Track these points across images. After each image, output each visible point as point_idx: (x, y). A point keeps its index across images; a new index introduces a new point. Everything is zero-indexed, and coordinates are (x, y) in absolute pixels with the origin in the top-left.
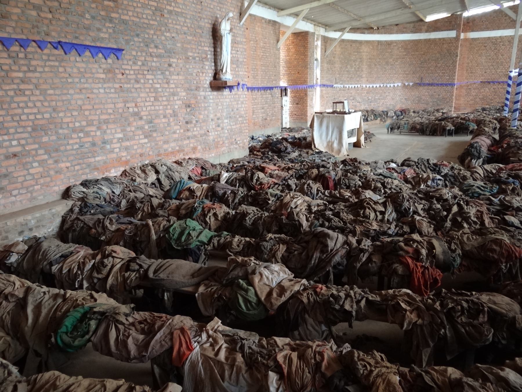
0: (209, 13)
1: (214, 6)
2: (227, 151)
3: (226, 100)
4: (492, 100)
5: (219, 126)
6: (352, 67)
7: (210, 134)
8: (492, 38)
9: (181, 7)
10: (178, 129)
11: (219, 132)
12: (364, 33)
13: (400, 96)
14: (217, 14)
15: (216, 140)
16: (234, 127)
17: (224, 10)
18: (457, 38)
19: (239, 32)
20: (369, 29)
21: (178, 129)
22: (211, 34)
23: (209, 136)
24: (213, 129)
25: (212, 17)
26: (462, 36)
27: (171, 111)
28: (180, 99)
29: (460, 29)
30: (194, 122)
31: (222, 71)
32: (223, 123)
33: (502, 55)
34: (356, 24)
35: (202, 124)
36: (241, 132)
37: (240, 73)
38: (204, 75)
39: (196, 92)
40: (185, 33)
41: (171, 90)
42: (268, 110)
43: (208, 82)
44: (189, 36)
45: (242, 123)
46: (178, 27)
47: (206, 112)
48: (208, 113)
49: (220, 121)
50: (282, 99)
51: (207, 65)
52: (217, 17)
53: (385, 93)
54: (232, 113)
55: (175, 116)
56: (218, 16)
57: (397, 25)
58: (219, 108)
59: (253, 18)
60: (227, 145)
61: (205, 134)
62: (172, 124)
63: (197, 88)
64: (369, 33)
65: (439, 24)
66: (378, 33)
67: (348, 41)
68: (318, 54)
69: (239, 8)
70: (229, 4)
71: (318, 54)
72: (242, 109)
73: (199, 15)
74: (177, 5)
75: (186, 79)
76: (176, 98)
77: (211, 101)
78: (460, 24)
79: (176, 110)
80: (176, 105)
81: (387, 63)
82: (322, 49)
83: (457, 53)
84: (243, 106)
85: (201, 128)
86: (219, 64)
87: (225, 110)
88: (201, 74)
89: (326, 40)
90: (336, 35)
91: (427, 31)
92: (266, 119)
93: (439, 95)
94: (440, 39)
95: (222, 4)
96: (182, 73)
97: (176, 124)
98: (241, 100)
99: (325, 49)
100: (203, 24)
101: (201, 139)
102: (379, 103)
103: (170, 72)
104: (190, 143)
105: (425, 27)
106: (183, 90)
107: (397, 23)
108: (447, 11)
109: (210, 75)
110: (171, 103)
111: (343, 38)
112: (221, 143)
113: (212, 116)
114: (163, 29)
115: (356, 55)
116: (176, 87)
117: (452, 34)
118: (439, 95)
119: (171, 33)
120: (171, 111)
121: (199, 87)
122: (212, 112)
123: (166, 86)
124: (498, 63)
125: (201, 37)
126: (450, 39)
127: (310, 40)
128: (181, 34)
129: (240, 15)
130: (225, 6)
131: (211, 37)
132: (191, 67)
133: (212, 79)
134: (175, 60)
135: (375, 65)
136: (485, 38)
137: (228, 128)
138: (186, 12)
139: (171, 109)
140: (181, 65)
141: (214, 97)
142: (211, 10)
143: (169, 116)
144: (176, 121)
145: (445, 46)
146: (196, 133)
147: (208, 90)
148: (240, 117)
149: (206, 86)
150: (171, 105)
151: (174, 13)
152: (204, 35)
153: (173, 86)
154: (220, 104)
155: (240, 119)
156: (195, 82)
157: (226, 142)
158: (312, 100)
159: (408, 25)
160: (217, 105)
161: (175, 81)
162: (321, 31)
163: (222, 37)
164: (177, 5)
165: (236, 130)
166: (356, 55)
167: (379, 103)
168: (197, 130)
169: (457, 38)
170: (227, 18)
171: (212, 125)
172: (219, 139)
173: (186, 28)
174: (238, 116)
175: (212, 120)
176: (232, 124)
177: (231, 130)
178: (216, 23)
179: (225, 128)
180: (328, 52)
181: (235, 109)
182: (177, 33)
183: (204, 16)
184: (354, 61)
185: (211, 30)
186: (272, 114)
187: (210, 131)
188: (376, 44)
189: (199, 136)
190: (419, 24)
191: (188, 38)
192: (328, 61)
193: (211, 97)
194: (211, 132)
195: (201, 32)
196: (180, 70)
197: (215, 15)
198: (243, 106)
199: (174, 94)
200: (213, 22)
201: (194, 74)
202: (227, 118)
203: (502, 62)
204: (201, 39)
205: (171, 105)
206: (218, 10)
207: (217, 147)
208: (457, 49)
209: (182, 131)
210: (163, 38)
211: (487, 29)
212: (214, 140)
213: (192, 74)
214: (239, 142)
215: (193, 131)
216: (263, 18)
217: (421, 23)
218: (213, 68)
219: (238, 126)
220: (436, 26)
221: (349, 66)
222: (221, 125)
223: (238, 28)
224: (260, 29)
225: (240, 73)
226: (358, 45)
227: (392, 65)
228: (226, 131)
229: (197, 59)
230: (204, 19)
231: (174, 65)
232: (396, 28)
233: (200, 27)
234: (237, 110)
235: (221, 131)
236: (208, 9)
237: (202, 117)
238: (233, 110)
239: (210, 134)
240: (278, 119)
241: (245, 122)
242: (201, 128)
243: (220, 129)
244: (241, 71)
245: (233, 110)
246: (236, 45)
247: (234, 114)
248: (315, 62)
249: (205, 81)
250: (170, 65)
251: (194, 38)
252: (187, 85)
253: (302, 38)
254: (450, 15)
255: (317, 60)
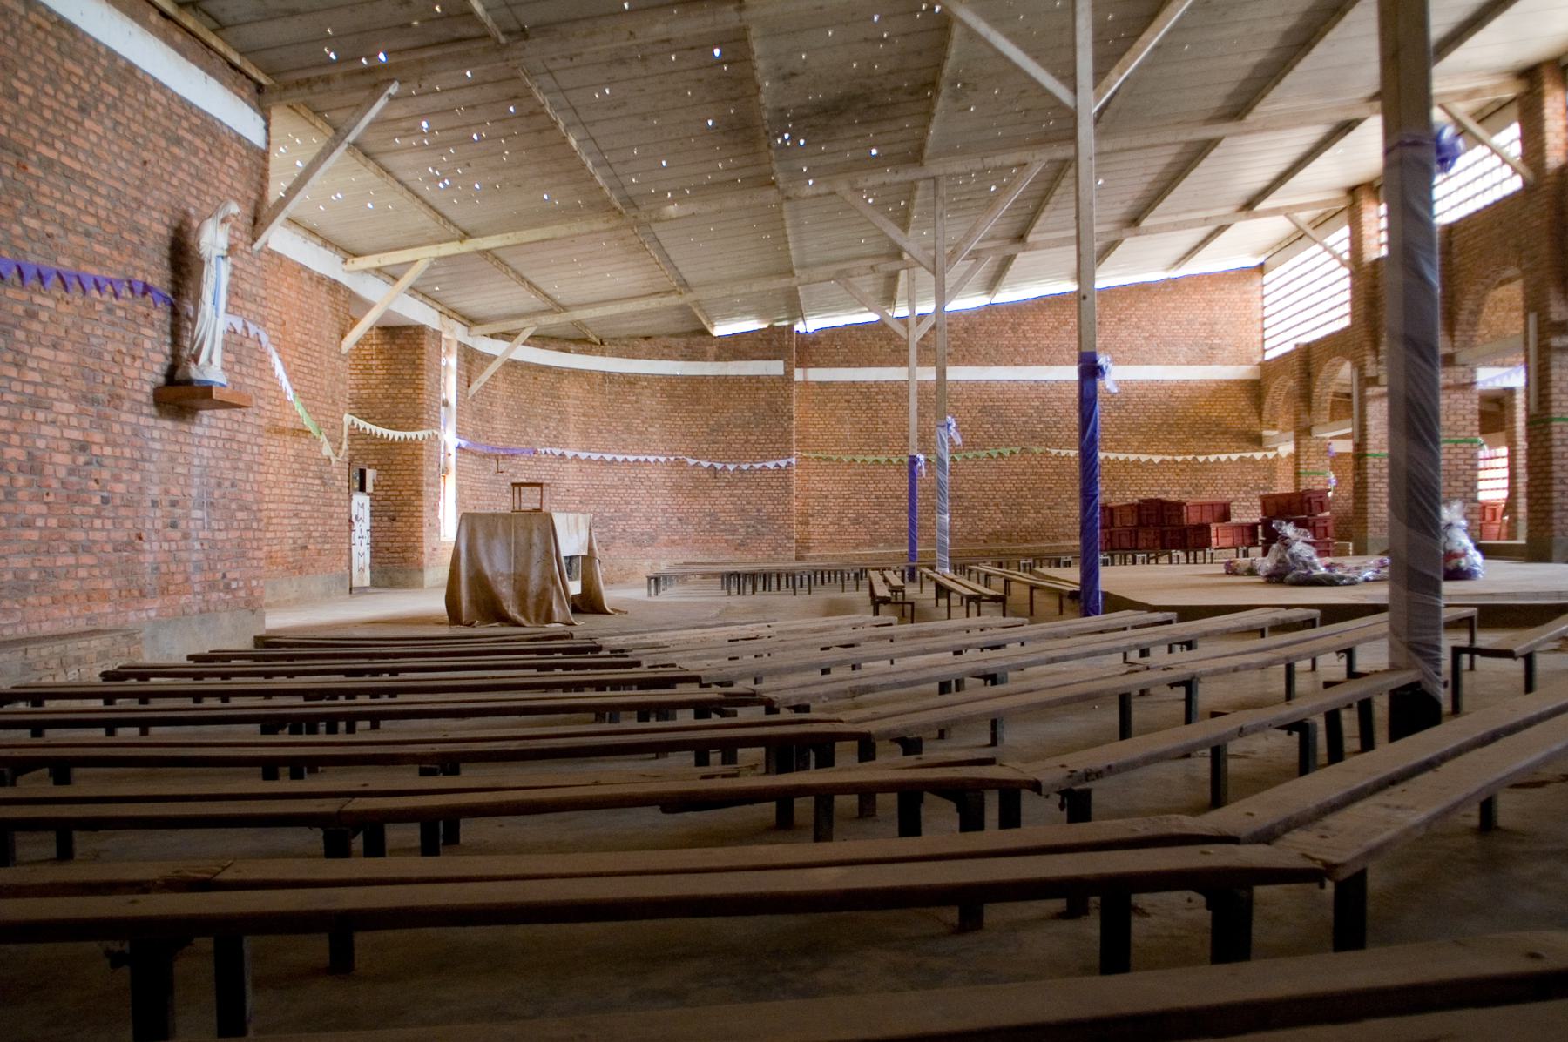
0: (165, 198)
1: (182, 181)
2: (196, 608)
3: (200, 451)
4: (875, 523)
5: (174, 525)
6: (538, 433)
7: (146, 546)
8: (861, 383)
9: (82, 157)
10: (41, 515)
11: (174, 545)
12: (568, 351)
13: (664, 511)
14: (189, 204)
15: (164, 568)
16: (222, 536)
17: (208, 199)
18: (787, 378)
19: (250, 269)
20: (580, 341)
21: (41, 515)
22: (167, 253)
23: (142, 551)
24: (157, 531)
25: (173, 209)
26: (798, 375)
27: (21, 455)
28: (53, 422)
29: (791, 358)
30: (97, 500)
31: (196, 361)
32: (187, 517)
33: (885, 423)
34: (551, 321)
35: (123, 512)
36: (243, 555)
37: (247, 381)
38: (138, 364)
39: (109, 411)
40: (88, 234)
41: (29, 390)
42: (310, 521)
43: (148, 388)
44: (99, 242)
45: (246, 529)
46: (69, 211)
47: (137, 477)
48: (143, 479)
49: (178, 511)
50: (350, 499)
51: (148, 337)
52: (186, 214)
53: (627, 503)
54: (217, 493)
55: (32, 470)
56: (192, 211)
57: (646, 338)
58: (179, 470)
59: (276, 261)
60: (198, 588)
61: (130, 543)
62: (23, 495)
63: (115, 399)
64: (578, 352)
65: (744, 345)
66: (603, 354)
67: (528, 366)
68: (450, 389)
69: (252, 204)
70: (223, 188)
71: (450, 389)
72: (248, 487)
73: (138, 195)
74: (70, 150)
75: (80, 365)
76: (41, 416)
77: (157, 446)
78: (789, 348)
79: (38, 453)
80: (41, 436)
81: (629, 429)
82: (459, 377)
83: (790, 411)
84: (251, 476)
85: (117, 523)
86: (187, 344)
87: (197, 480)
88: (128, 360)
89: (471, 360)
90: (497, 348)
91: (717, 359)
92: (305, 548)
93: (759, 511)
94: (749, 378)
95: (202, 181)
96: (68, 345)
97: (36, 499)
98: (246, 457)
99: (466, 378)
100: (147, 223)
101: (114, 557)
102: (614, 530)
103: (28, 332)
104: (78, 566)
105: (712, 350)
106: (65, 396)
107: (646, 332)
108: (761, 315)
109: (157, 368)
110: (24, 428)
111: (513, 356)
112: (179, 578)
113: (154, 491)
114: (19, 204)
115: (548, 404)
116: (47, 384)
117: (776, 368)
118: (759, 511)
119: (44, 221)
120: (21, 455)
121: (119, 397)
122: (155, 478)
123: (13, 373)
124: (877, 440)
125: (135, 253)
126: (772, 378)
127: (429, 347)
128: (77, 232)
129: (255, 220)
130: (212, 190)
131: (166, 263)
132: (99, 332)
133: (161, 380)
134: (50, 303)
135: (600, 432)
136: (844, 383)
137: (201, 535)
138: (98, 176)
139: (21, 447)
140: (68, 321)
141: (165, 435)
142: (171, 190)
143: (12, 467)
144: (35, 489)
145: (763, 394)
146: (98, 536)
147: (146, 410)
148: (242, 508)
149: (143, 398)
150: (23, 436)
151: (57, 169)
152: (143, 249)
153: (37, 378)
154: (181, 460)
155: (240, 515)
156: (108, 380)
157: (197, 577)
158: (435, 508)
159: (674, 340)
160: (172, 460)
161: (45, 365)
162: (455, 333)
163: (202, 262)
164: (70, 150)
165: (228, 545)
166: (548, 404)
167: (614, 530)
168: (103, 529)
169: (787, 378)
170: (221, 216)
171: (155, 520)
172: (173, 567)
173: (92, 221)
174: (234, 506)
175: (155, 504)
176: (214, 525)
177: (213, 544)
178: (185, 228)
179: (194, 534)
180: (475, 387)
181: (227, 484)
182: (62, 225)
183: (150, 202)
184: (544, 419)
185: (168, 243)
186: (324, 536)
187: (144, 535)
188: (599, 380)
189: (109, 547)
190: (695, 340)
191: (97, 247)
192: (474, 411)
193: (156, 434)
194: (151, 541)
195: (136, 239)
196: (62, 334)
197: (184, 206)
198: (251, 476)
199: (36, 404)
200: (175, 224)
201: (107, 357)
202: (201, 506)
203: (886, 438)
204: (137, 262)
205: (23, 436)
206: (190, 194)
207: (164, 591)
208: (790, 403)
209: (53, 522)
210: (17, 230)
211: (847, 363)
212: (157, 568)
213: (100, 356)
214: (234, 585)
215: (92, 528)
216: (304, 268)
217: (703, 339)
218: (167, 349)
219: (233, 534)
220: (736, 347)
221: (530, 430)
222: (182, 524)
223: (245, 256)
224: (292, 294)
225: (247, 381)
226: (552, 378)
227: (640, 433)
228: (197, 546)
229: (121, 313)
230: (149, 208)
231: (44, 316)
232: (645, 345)
233: (136, 230)
234: (233, 485)
235: (182, 544)
236: (164, 185)
237: (120, 488)
238: (219, 485)
239: (146, 546)
240: (340, 552)
241: (255, 525)
242: (117, 523)
243: (177, 535)
244: (249, 376)
245: (219, 485)
246: (239, 302)
247: (224, 496)
248: (443, 409)
249: (138, 383)
250: (32, 315)
251: (115, 253)
252: (79, 385)
253: (400, 341)
254: (765, 326)
255: (446, 404)
